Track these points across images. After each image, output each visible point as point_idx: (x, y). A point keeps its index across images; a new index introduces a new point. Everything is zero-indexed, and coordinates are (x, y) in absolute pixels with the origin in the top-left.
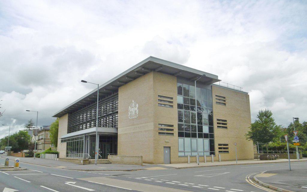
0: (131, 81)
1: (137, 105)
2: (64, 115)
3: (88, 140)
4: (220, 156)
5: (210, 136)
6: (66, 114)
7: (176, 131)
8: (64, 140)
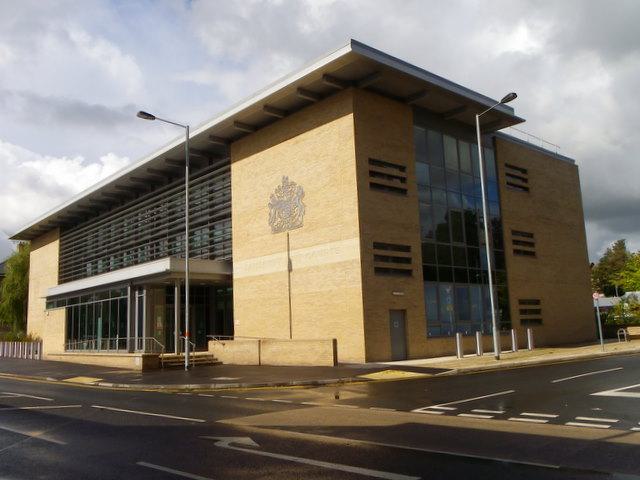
0: (276, 119)
3: (141, 299)
6: (54, 228)
7: (417, 265)
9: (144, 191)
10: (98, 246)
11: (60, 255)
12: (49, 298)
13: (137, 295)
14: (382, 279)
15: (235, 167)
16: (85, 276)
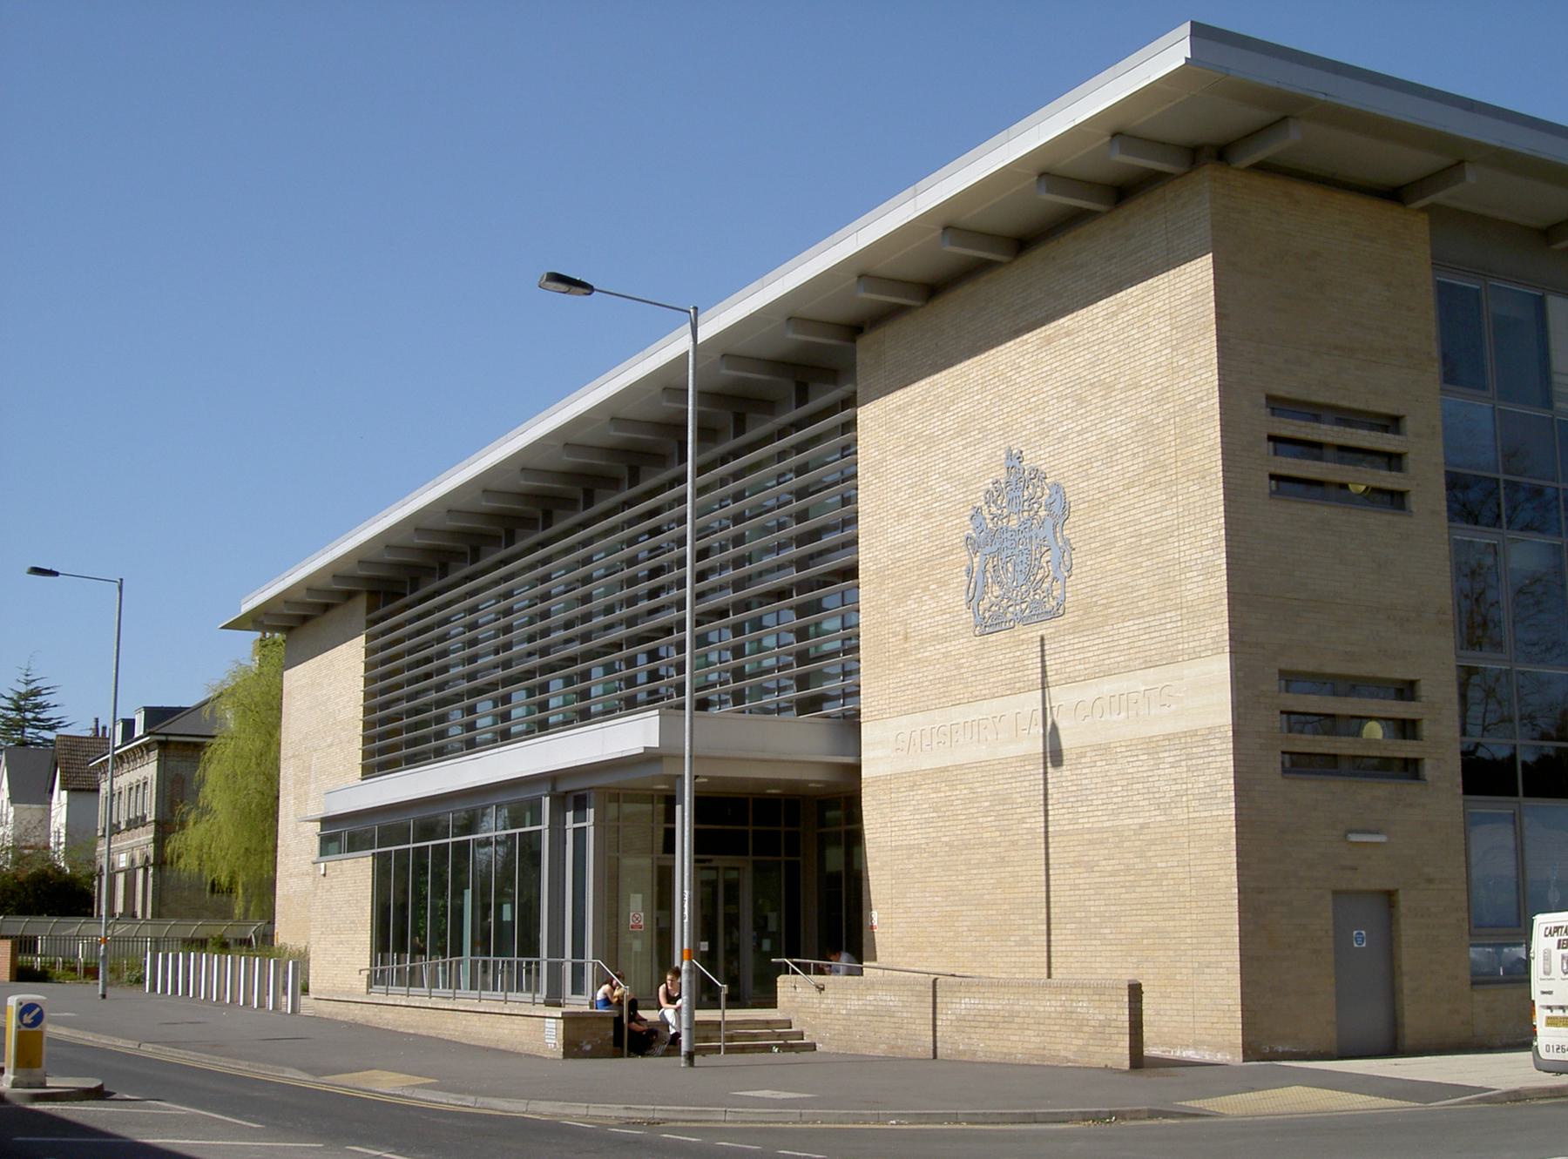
3: (580, 834)
6: (350, 595)
9: (611, 482)
10: (545, 633)
11: (368, 681)
12: (326, 822)
13: (570, 824)
14: (1310, 790)
15: (868, 415)
16: (440, 754)
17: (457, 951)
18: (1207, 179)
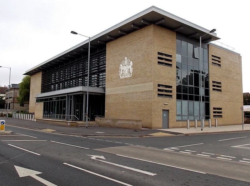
1: (131, 63)
2: (36, 73)
3: (71, 101)
4: (216, 121)
5: (207, 99)
6: (39, 71)
8: (41, 100)
17: (200, 101)
18: (152, 26)
